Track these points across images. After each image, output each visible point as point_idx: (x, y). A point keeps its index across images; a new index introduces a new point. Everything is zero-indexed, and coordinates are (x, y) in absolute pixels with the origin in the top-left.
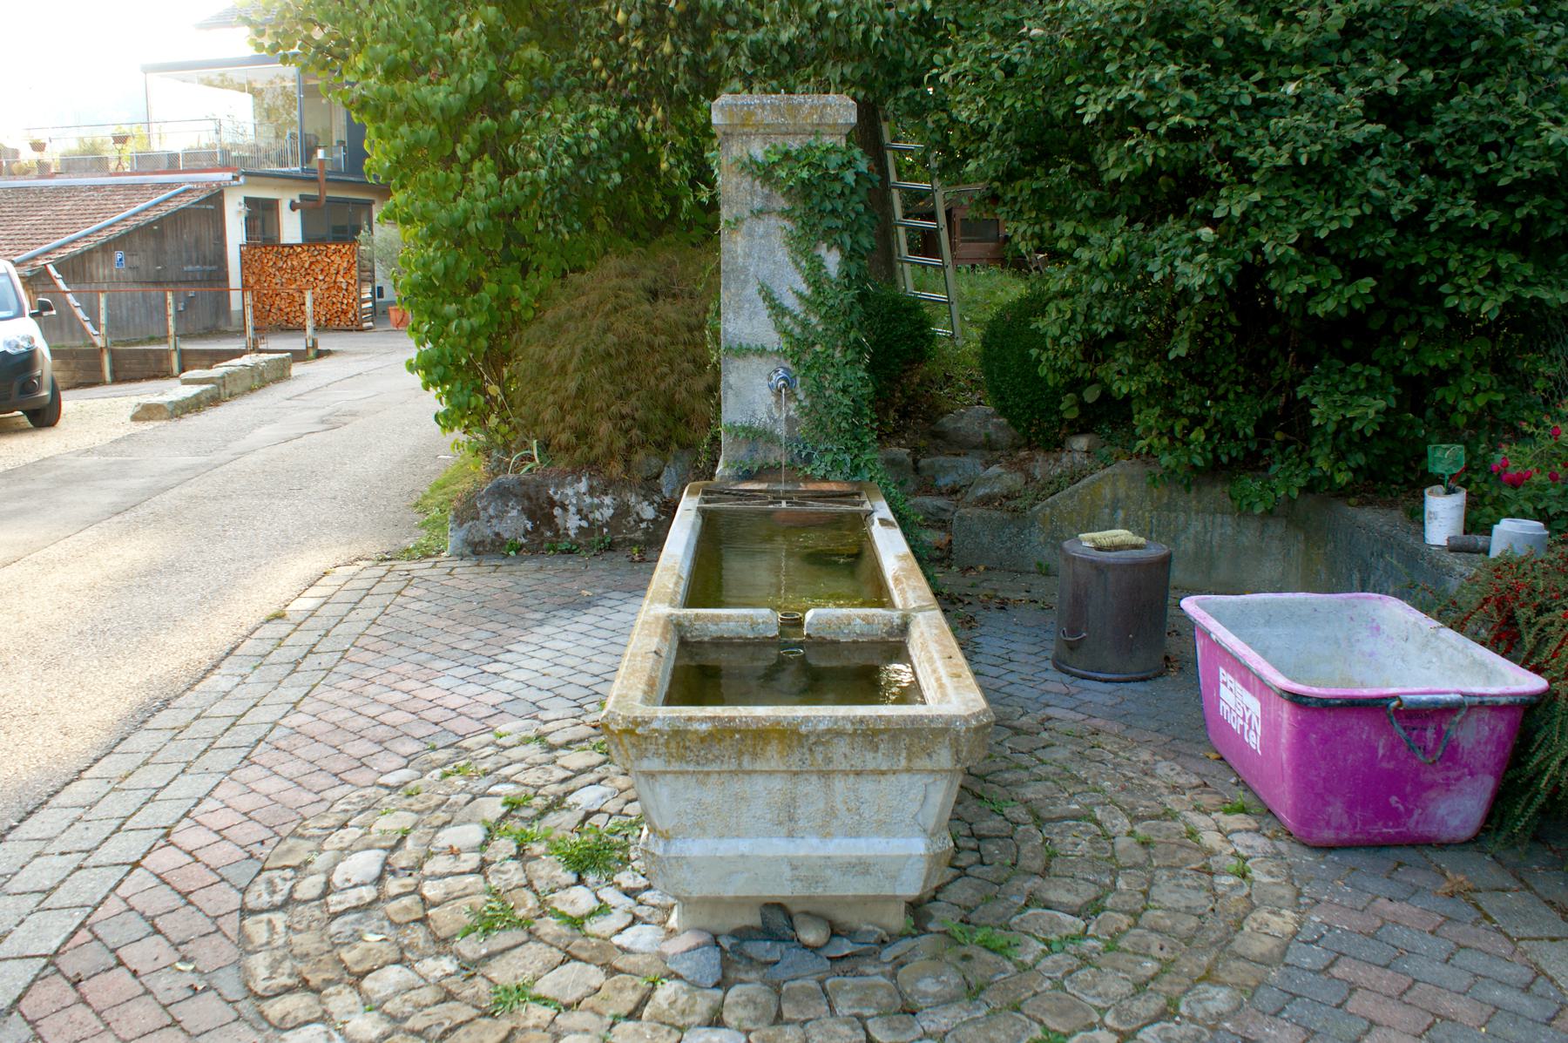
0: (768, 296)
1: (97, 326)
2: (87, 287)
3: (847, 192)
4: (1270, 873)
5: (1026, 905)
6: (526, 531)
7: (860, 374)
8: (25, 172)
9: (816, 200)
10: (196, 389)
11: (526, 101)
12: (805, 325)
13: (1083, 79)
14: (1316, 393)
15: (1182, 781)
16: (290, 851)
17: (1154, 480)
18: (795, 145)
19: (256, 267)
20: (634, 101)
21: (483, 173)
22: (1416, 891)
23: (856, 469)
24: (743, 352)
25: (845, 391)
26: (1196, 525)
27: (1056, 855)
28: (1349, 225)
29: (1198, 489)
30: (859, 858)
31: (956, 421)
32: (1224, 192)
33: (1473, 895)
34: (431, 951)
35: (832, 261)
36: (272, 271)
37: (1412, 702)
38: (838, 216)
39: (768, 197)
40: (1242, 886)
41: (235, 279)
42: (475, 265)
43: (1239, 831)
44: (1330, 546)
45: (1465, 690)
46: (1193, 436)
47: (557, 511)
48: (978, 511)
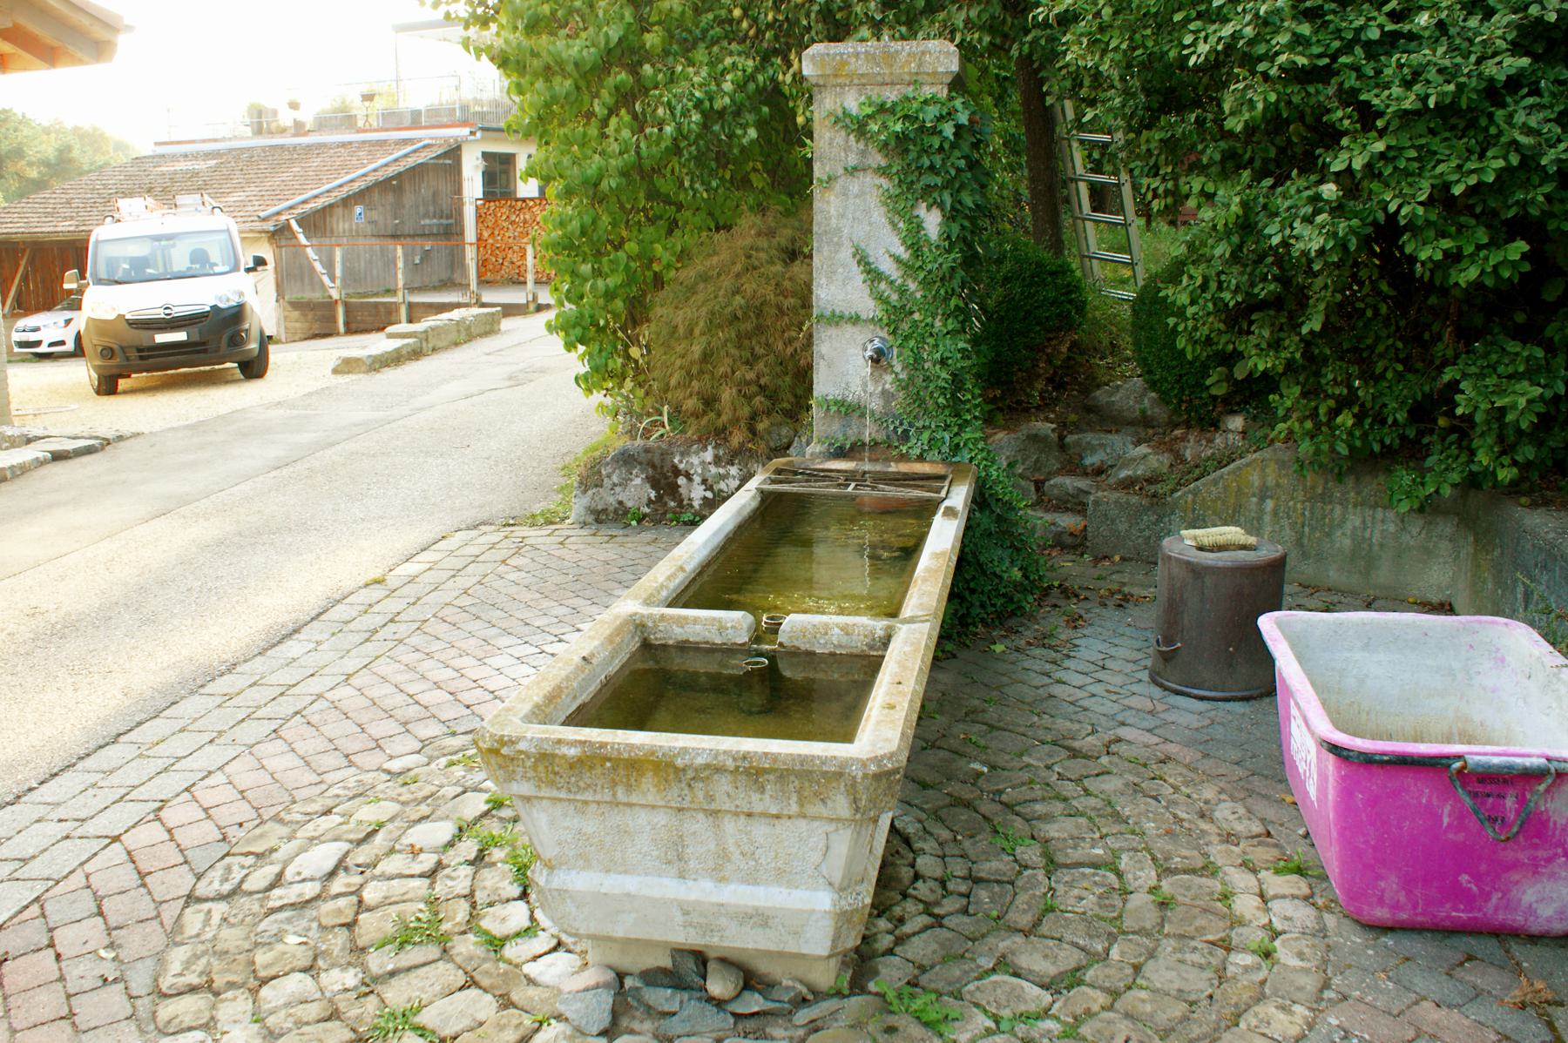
0: (863, 261)
1: (333, 280)
2: (327, 241)
3: (946, 146)
4: (1300, 955)
5: (993, 970)
6: (650, 502)
7: (961, 345)
8: (283, 131)
9: (912, 155)
10: (398, 343)
11: (666, 53)
12: (902, 291)
13: (1194, 14)
14: (1465, 376)
15: (1239, 827)
16: (261, 836)
17: (1302, 466)
18: (891, 96)
19: (490, 221)
20: (776, 52)
21: (620, 127)
22: (1478, 994)
23: (956, 449)
24: (836, 319)
25: (943, 362)
26: (1354, 520)
27: (1052, 909)
28: (1490, 178)
29: (1357, 480)
30: (756, 909)
31: (1111, 395)
32: (1345, 142)
33: (1550, 1009)
34: (343, 961)
35: (932, 222)
36: (505, 224)
37: (1478, 764)
38: (937, 174)
39: (863, 153)
40: (1259, 968)
41: (470, 234)
42: (614, 224)
43: (1284, 897)
44: (1497, 553)
45: (1552, 753)
46: (1339, 420)
47: (681, 481)
48: (1115, 495)
